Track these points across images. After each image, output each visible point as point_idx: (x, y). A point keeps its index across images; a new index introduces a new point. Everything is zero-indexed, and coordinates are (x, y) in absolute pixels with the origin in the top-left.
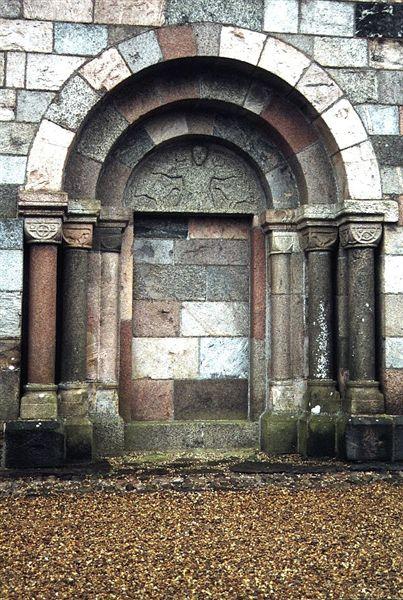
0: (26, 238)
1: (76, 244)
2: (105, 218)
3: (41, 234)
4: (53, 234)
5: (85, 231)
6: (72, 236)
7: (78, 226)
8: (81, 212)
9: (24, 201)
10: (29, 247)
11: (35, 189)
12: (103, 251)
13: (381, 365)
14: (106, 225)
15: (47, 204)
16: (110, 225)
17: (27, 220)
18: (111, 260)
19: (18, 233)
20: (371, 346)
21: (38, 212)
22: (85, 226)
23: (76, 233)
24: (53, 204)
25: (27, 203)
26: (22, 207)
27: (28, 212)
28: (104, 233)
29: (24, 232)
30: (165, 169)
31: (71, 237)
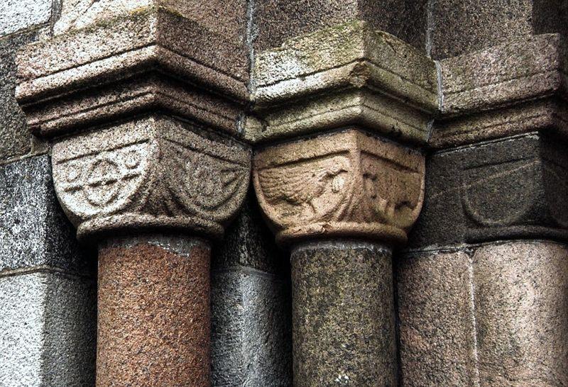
0: (61, 220)
1: (302, 222)
2: (462, 101)
3: (95, 196)
4: (133, 186)
5: (331, 165)
6: (289, 191)
7: (305, 149)
8: (294, 86)
9: (29, 78)
10: (78, 254)
11: (80, 25)
12: (477, 242)
13: (276, 145)
14: (473, 130)
15: (94, 69)
16: (489, 126)
17: (61, 151)
18: (512, 272)
19: (32, 209)
20: (186, 126)
21: (78, 112)
22: (327, 144)
23: (303, 179)
24: (110, 64)
25: (41, 84)
26: (34, 104)
27: (53, 119)
28: (480, 165)
29: (54, 203)
30: (281, 192)
31: (285, 199)
